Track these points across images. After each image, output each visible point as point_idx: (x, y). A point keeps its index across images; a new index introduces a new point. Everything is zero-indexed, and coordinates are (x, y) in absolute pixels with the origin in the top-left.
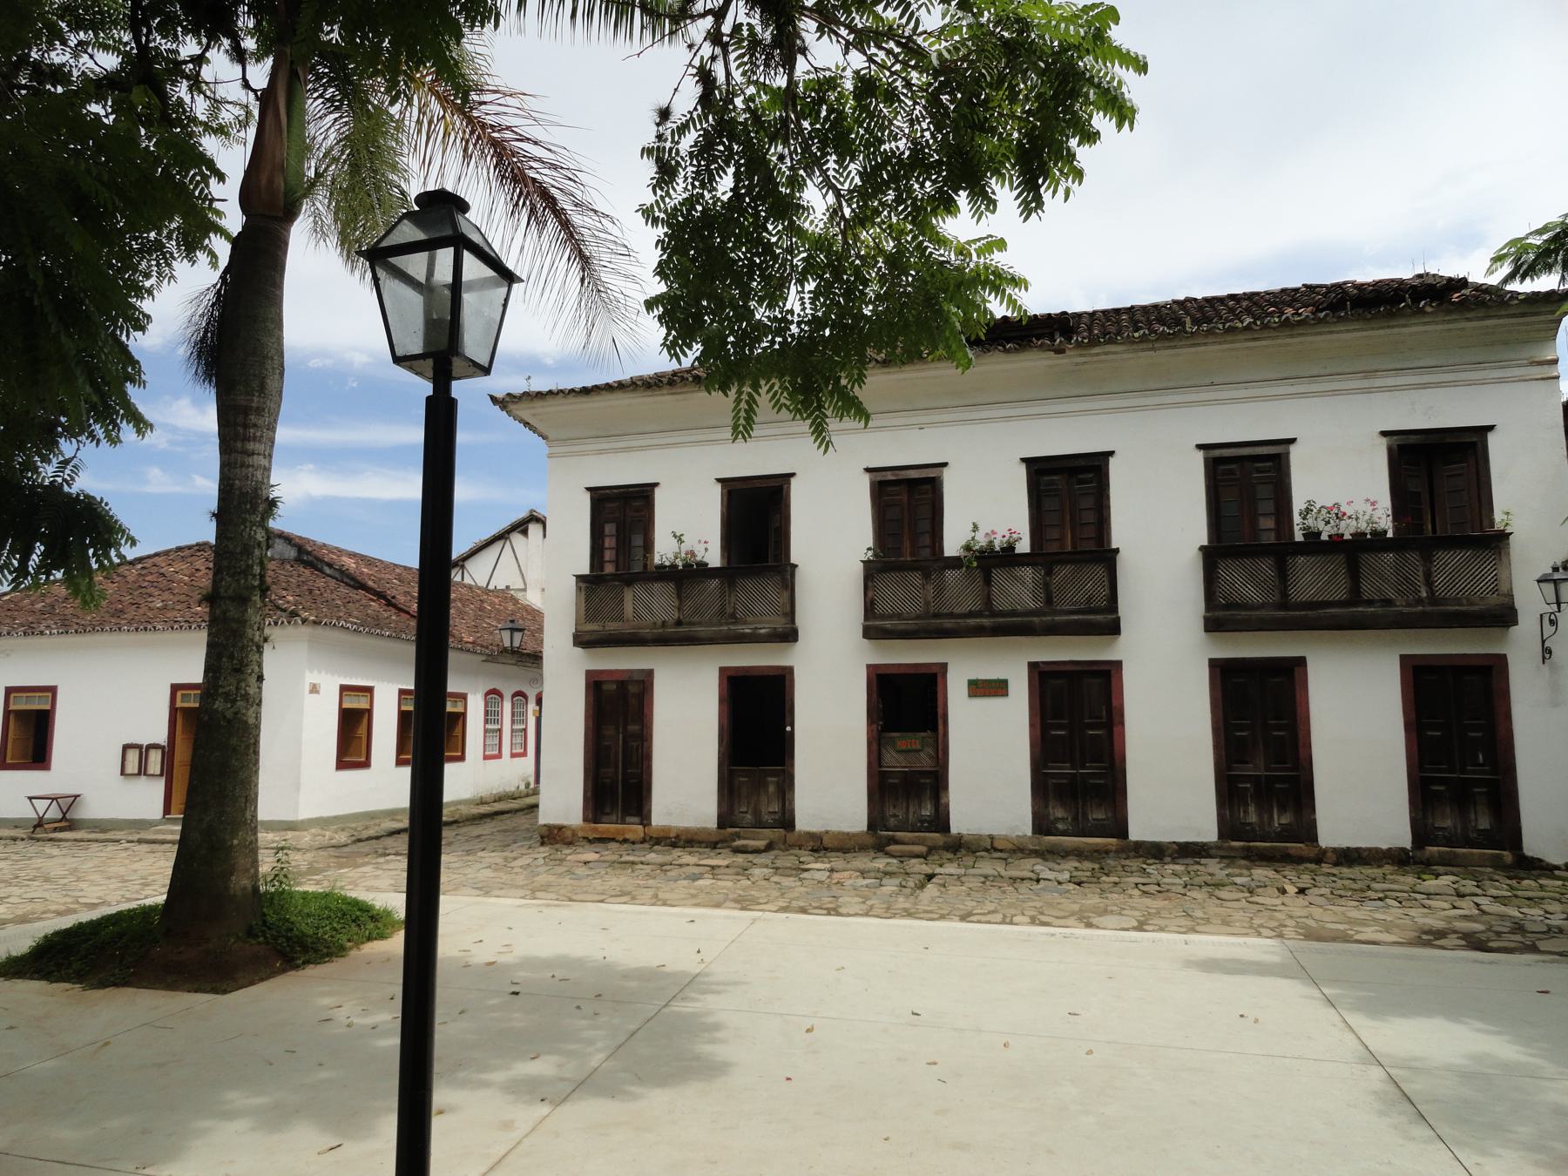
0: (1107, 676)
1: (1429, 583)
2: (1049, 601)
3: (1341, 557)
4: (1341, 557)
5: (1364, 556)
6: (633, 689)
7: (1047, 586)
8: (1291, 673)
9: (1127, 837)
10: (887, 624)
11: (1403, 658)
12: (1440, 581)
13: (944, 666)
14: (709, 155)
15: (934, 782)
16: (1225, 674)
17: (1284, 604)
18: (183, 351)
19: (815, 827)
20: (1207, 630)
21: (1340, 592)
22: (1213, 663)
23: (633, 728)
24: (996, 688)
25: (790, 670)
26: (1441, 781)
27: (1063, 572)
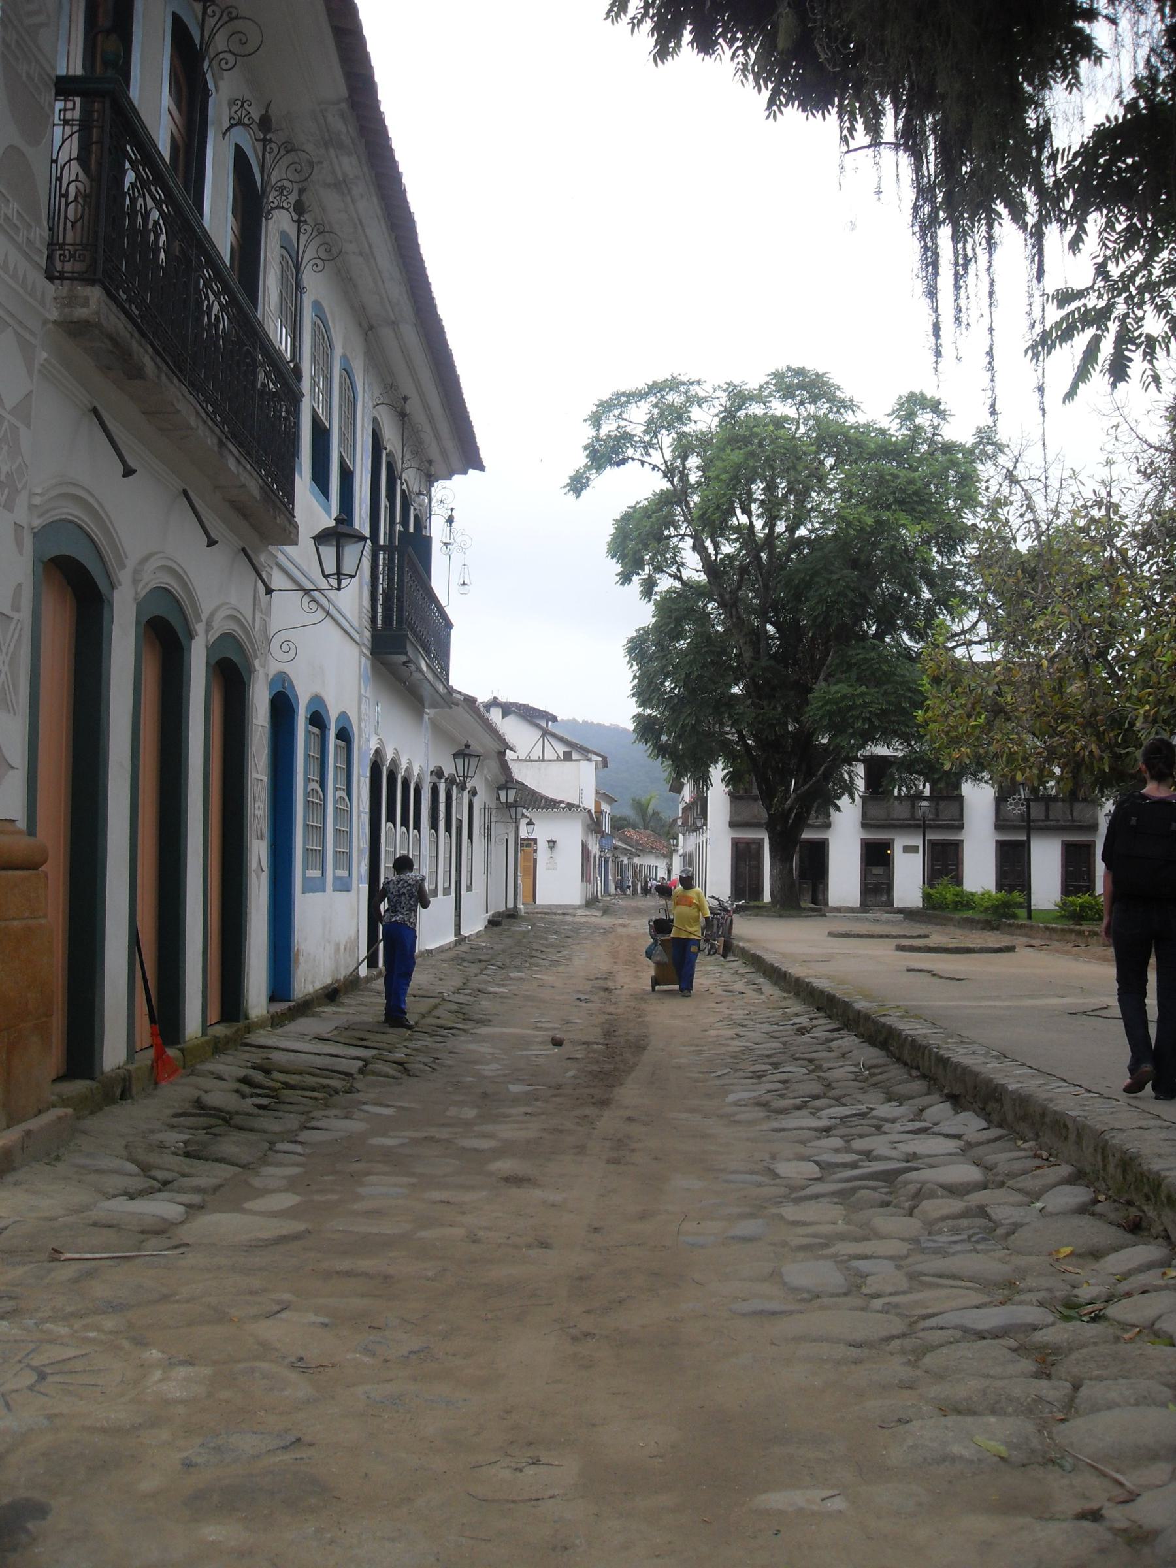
0: (957, 846)
1: (1072, 815)
2: (937, 815)
3: (1043, 803)
4: (1043, 803)
5: (1051, 803)
6: (754, 846)
7: (937, 810)
8: (888, 845)
9: (893, 905)
10: (872, 822)
11: (1063, 841)
12: (1075, 814)
13: (893, 840)
14: (1156, 582)
15: (889, 887)
16: (736, 844)
17: (913, 818)
18: (368, 692)
19: (901, 906)
20: (730, 826)
21: (907, 815)
22: (997, 841)
23: (754, 863)
24: (914, 849)
25: (827, 839)
26: (1072, 885)
27: (942, 804)
